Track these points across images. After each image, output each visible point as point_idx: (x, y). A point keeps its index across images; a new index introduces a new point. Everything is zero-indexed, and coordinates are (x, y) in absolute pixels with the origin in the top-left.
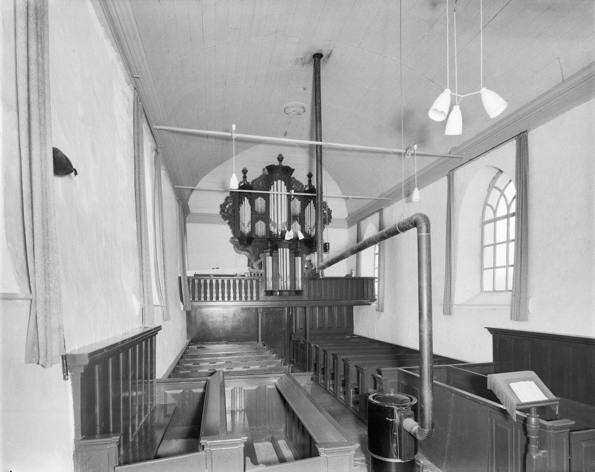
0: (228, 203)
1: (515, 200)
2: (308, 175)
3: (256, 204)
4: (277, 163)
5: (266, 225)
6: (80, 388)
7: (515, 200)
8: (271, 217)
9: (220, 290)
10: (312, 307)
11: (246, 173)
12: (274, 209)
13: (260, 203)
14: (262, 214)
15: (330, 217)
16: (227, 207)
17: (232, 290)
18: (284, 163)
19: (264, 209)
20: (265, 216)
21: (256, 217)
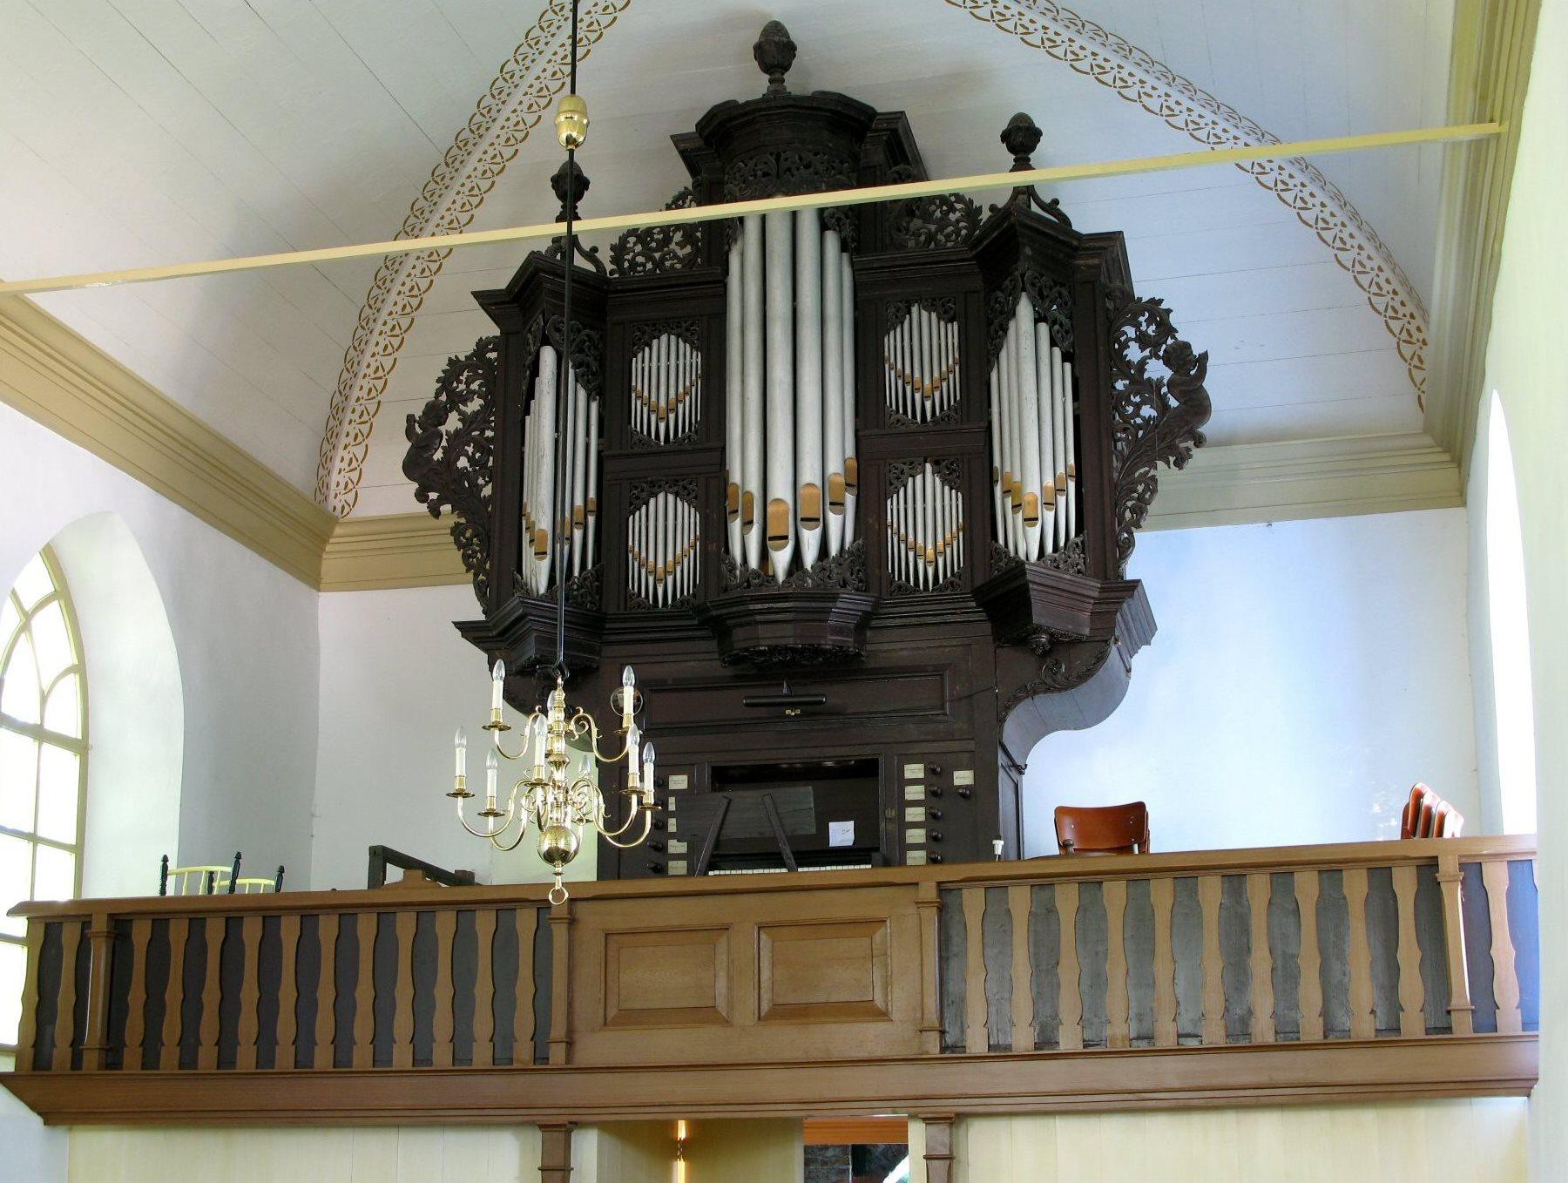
0: (456, 400)
1: (593, 269)
2: (1006, 137)
3: (636, 382)
4: (752, 85)
5: (705, 524)
6: (1541, 924)
7: (593, 269)
8: (743, 470)
9: (364, 994)
10: (1390, 1036)
11: (579, 196)
12: (588, 434)
13: (663, 372)
14: (676, 448)
15: (1196, 405)
16: (453, 423)
17: (443, 992)
18: (798, 82)
19: (688, 410)
20: (695, 465)
21: (632, 468)
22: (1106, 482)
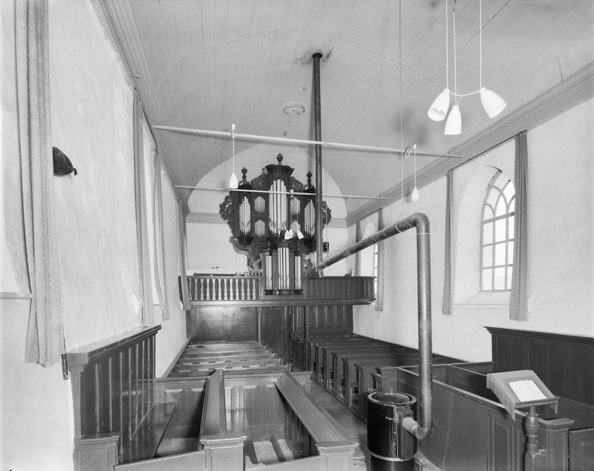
0: (228, 203)
1: (514, 200)
2: (307, 175)
3: (255, 203)
4: (276, 163)
5: (266, 224)
7: (514, 200)
8: (271, 216)
9: (220, 290)
11: (246, 173)
12: (273, 208)
13: (259, 202)
14: (261, 214)
15: (330, 217)
16: (227, 206)
17: (231, 290)
18: (284, 163)
19: (263, 209)
20: (264, 216)
21: (256, 216)
22: (200, 277)
